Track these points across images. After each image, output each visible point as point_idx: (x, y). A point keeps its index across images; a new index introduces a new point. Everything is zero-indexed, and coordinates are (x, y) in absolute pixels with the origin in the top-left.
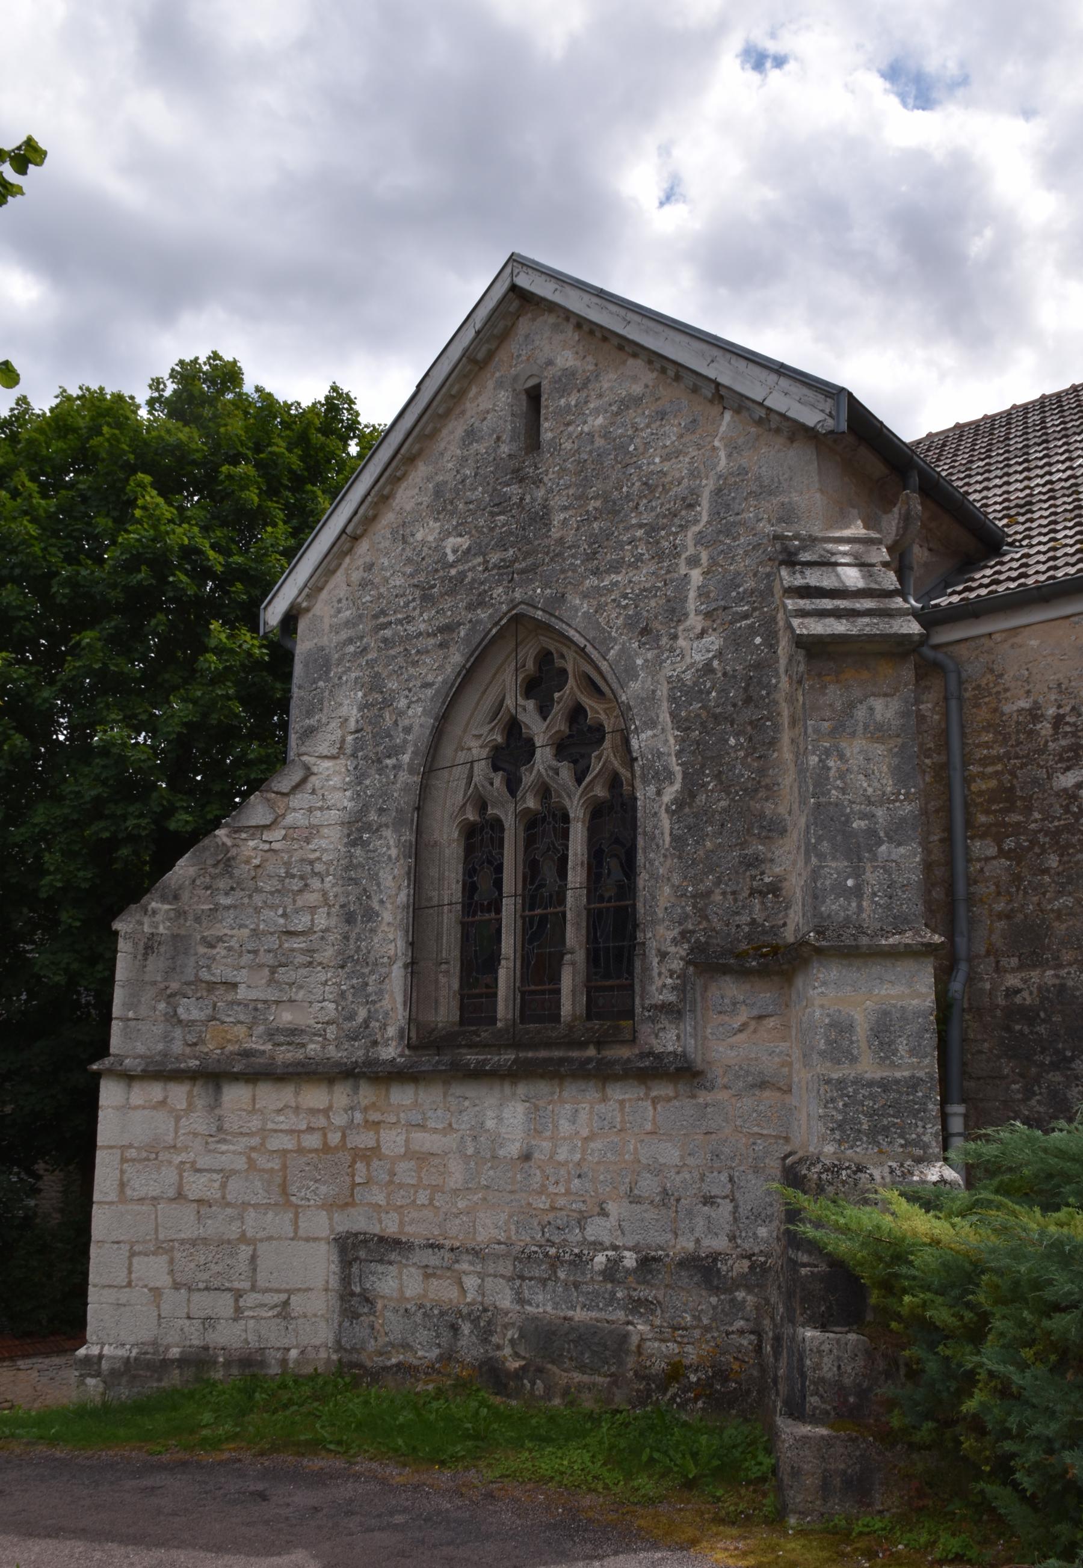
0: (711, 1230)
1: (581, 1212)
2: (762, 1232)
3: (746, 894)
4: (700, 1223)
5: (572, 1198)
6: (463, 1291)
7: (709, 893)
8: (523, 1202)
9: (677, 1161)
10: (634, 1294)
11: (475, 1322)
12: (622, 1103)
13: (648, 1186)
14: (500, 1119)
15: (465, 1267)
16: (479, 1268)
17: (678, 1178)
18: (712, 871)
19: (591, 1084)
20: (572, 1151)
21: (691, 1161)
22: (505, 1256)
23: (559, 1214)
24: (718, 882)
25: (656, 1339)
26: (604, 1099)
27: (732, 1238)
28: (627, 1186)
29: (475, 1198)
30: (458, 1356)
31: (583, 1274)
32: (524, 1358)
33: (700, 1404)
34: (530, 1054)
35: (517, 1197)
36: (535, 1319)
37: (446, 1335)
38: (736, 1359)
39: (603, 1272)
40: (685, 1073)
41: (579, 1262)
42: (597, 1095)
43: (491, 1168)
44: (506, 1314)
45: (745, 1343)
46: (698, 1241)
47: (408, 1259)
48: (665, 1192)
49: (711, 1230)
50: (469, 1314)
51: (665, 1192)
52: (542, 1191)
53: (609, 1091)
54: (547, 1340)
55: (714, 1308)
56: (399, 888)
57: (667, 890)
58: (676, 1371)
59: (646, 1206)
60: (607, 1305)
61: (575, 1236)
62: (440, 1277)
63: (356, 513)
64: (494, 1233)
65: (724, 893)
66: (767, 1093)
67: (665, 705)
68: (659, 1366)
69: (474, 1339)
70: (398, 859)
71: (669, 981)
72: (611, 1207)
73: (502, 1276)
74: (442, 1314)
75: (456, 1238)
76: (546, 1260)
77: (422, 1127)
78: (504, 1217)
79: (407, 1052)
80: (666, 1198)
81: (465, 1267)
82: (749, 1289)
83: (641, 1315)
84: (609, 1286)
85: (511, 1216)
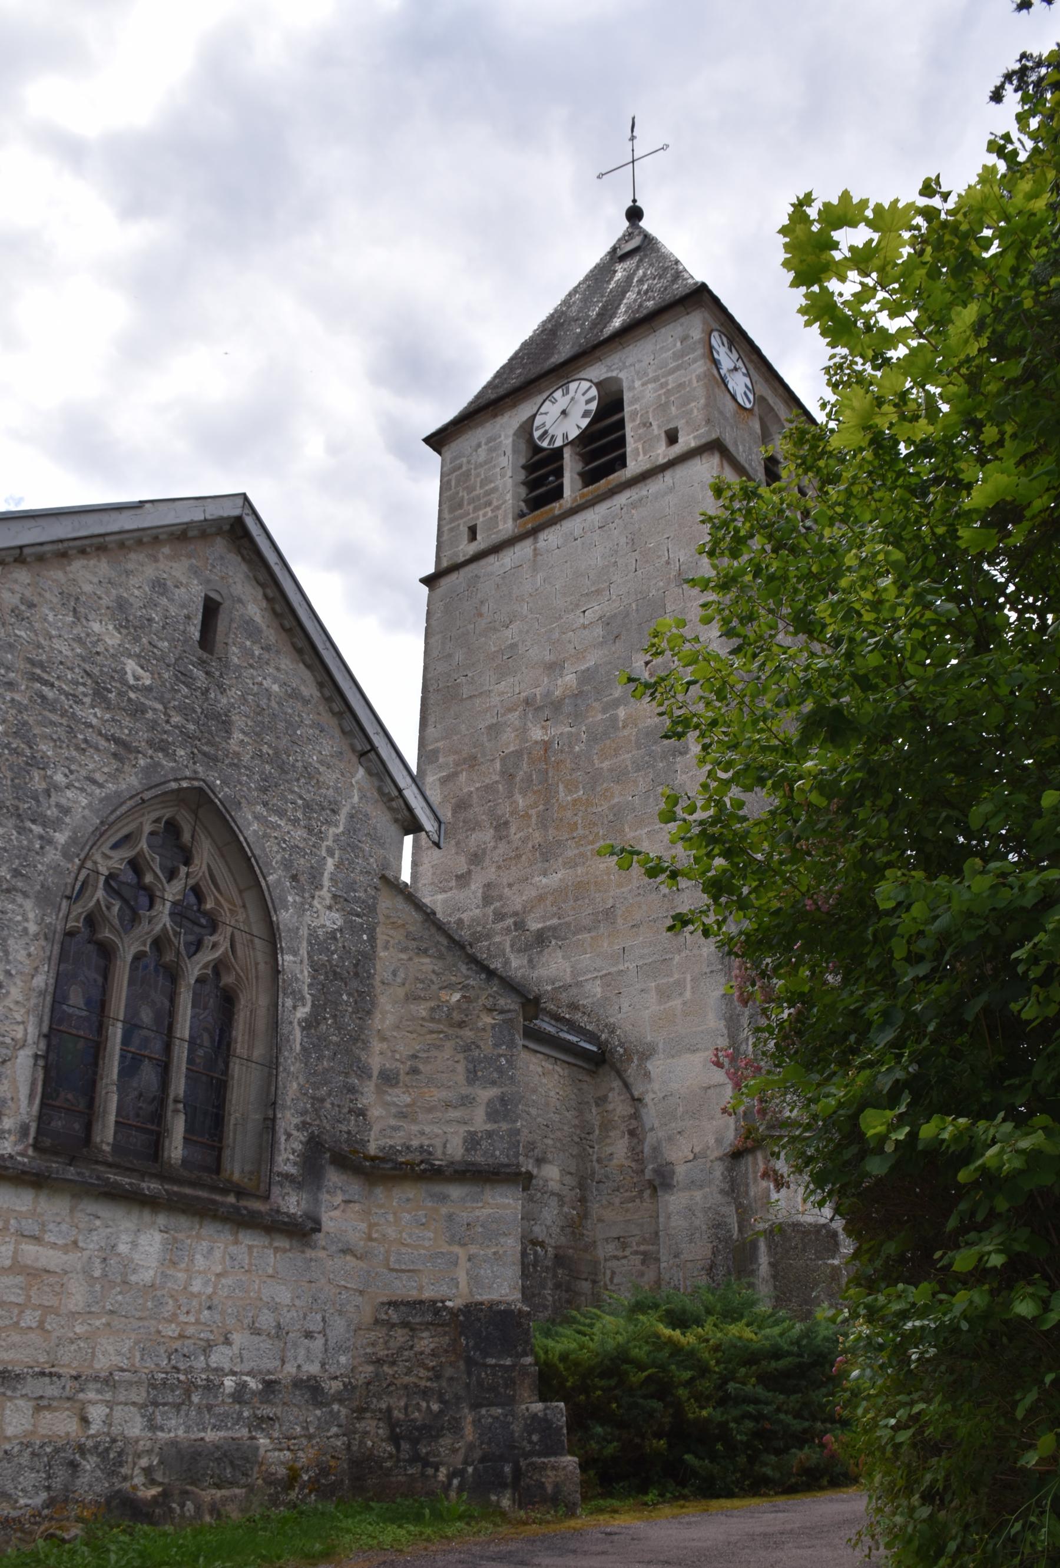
0: (309, 1359)
1: (208, 1340)
2: (343, 1359)
3: (346, 1110)
4: (302, 1352)
5: (201, 1327)
6: (85, 1421)
7: (322, 1100)
8: (153, 1330)
9: (288, 1301)
10: (259, 1412)
11: (104, 1455)
12: (250, 1247)
13: (266, 1320)
14: (134, 1244)
15: (92, 1395)
16: (108, 1396)
17: (289, 1315)
18: (325, 1084)
19: (228, 1227)
20: (206, 1283)
21: (297, 1302)
22: (139, 1383)
23: (187, 1342)
24: (329, 1094)
25: (275, 1450)
26: (236, 1242)
27: (323, 1365)
28: (250, 1320)
29: (98, 1323)
30: (76, 1495)
31: (216, 1397)
32: (160, 1484)
33: (313, 1497)
34: (175, 1189)
35: (146, 1323)
36: (174, 1443)
37: (61, 1475)
38: (333, 1457)
39: (232, 1395)
40: (301, 1231)
41: (211, 1387)
42: (231, 1238)
43: (120, 1293)
44: (137, 1442)
45: (339, 1443)
46: (299, 1366)
47: (15, 1389)
48: (279, 1326)
49: (309, 1359)
50: (96, 1447)
51: (279, 1326)
52: (173, 1319)
53: (241, 1236)
54: (189, 1464)
55: (319, 1419)
56: (36, 969)
57: (295, 1085)
58: (293, 1477)
59: (264, 1337)
60: (234, 1424)
61: (200, 1363)
62: (56, 1409)
63: (41, 544)
64: (116, 1360)
65: (333, 1104)
66: (348, 1258)
67: (305, 944)
68: (282, 1471)
69: (99, 1473)
70: (36, 937)
71: (291, 1157)
72: (236, 1337)
73: (134, 1404)
74: (57, 1450)
75: (69, 1366)
76: (172, 1388)
77: (37, 1239)
78: (129, 1343)
79: (30, 1152)
80: (280, 1332)
81: (92, 1395)
82: (341, 1402)
83: (263, 1430)
84: (237, 1407)
85: (136, 1343)
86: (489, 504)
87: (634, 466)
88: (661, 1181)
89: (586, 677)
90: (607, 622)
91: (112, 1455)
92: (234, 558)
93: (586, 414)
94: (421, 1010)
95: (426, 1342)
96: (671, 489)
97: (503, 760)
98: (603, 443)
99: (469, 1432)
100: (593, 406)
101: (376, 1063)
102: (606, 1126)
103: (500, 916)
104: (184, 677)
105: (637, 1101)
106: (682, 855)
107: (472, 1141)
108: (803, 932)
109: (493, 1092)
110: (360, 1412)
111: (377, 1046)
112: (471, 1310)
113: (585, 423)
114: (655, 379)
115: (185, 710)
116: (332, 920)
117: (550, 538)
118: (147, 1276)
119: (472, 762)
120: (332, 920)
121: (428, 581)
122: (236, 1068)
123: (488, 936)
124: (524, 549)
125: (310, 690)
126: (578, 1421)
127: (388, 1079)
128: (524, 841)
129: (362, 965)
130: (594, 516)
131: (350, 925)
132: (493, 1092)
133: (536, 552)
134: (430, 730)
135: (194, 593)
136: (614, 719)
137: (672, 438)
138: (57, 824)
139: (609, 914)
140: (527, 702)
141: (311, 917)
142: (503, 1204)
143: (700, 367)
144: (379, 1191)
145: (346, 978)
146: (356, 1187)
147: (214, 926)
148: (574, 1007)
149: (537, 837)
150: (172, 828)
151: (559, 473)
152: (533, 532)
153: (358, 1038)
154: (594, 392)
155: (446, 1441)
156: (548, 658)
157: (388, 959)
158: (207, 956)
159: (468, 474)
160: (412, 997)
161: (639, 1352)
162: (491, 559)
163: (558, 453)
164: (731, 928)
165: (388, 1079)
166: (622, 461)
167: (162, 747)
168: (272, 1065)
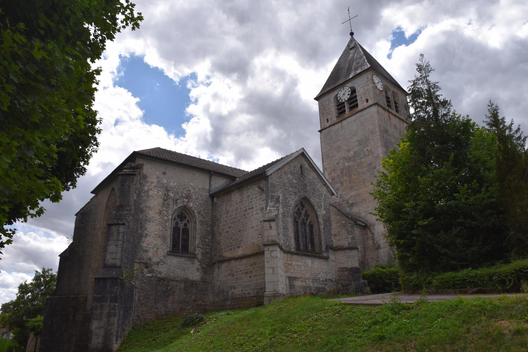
40: (327, 258)
41: (319, 280)
58: (330, 292)
80: (326, 273)
86: (330, 114)
87: (360, 107)
88: (378, 247)
89: (355, 153)
90: (358, 141)
91: (310, 288)
92: (302, 158)
93: (349, 95)
94: (339, 224)
95: (346, 273)
96: (368, 113)
97: (341, 170)
98: (353, 101)
99: (354, 285)
100: (350, 93)
101: (333, 233)
102: (368, 239)
103: (344, 201)
104: (300, 180)
105: (373, 234)
106: (377, 213)
107: (349, 244)
108: (393, 213)
109: (351, 236)
110: (338, 283)
111: (333, 230)
112: (352, 268)
113: (349, 97)
114: (362, 87)
115: (301, 185)
116: (324, 212)
117: (344, 123)
118: (310, 265)
119: (334, 170)
120: (324, 212)
121: (319, 131)
122: (315, 236)
123: (342, 205)
124: (339, 125)
125: (316, 176)
126: (369, 283)
127: (335, 235)
128: (347, 186)
129: (329, 218)
130: (353, 118)
131: (327, 213)
132: (351, 236)
133: (342, 126)
134: (325, 163)
135: (299, 166)
136: (362, 161)
137: (367, 101)
138: (290, 206)
139: (364, 200)
140: (344, 158)
141: (321, 212)
142: (355, 252)
143: (371, 85)
144: (336, 252)
145: (328, 221)
146: (333, 252)
147: (309, 216)
148: (360, 217)
149: (349, 185)
150: (302, 203)
151: (344, 107)
152: (341, 121)
153: (330, 230)
154: (350, 90)
155: (350, 287)
156: (347, 149)
157: (333, 217)
158: (309, 221)
159: (324, 107)
160: (337, 223)
161: (377, 273)
162: (332, 127)
163: (344, 103)
164: (383, 220)
165: (335, 235)
166: (357, 106)
167: (300, 192)
168: (320, 236)
